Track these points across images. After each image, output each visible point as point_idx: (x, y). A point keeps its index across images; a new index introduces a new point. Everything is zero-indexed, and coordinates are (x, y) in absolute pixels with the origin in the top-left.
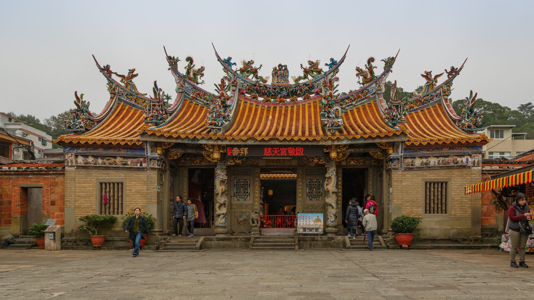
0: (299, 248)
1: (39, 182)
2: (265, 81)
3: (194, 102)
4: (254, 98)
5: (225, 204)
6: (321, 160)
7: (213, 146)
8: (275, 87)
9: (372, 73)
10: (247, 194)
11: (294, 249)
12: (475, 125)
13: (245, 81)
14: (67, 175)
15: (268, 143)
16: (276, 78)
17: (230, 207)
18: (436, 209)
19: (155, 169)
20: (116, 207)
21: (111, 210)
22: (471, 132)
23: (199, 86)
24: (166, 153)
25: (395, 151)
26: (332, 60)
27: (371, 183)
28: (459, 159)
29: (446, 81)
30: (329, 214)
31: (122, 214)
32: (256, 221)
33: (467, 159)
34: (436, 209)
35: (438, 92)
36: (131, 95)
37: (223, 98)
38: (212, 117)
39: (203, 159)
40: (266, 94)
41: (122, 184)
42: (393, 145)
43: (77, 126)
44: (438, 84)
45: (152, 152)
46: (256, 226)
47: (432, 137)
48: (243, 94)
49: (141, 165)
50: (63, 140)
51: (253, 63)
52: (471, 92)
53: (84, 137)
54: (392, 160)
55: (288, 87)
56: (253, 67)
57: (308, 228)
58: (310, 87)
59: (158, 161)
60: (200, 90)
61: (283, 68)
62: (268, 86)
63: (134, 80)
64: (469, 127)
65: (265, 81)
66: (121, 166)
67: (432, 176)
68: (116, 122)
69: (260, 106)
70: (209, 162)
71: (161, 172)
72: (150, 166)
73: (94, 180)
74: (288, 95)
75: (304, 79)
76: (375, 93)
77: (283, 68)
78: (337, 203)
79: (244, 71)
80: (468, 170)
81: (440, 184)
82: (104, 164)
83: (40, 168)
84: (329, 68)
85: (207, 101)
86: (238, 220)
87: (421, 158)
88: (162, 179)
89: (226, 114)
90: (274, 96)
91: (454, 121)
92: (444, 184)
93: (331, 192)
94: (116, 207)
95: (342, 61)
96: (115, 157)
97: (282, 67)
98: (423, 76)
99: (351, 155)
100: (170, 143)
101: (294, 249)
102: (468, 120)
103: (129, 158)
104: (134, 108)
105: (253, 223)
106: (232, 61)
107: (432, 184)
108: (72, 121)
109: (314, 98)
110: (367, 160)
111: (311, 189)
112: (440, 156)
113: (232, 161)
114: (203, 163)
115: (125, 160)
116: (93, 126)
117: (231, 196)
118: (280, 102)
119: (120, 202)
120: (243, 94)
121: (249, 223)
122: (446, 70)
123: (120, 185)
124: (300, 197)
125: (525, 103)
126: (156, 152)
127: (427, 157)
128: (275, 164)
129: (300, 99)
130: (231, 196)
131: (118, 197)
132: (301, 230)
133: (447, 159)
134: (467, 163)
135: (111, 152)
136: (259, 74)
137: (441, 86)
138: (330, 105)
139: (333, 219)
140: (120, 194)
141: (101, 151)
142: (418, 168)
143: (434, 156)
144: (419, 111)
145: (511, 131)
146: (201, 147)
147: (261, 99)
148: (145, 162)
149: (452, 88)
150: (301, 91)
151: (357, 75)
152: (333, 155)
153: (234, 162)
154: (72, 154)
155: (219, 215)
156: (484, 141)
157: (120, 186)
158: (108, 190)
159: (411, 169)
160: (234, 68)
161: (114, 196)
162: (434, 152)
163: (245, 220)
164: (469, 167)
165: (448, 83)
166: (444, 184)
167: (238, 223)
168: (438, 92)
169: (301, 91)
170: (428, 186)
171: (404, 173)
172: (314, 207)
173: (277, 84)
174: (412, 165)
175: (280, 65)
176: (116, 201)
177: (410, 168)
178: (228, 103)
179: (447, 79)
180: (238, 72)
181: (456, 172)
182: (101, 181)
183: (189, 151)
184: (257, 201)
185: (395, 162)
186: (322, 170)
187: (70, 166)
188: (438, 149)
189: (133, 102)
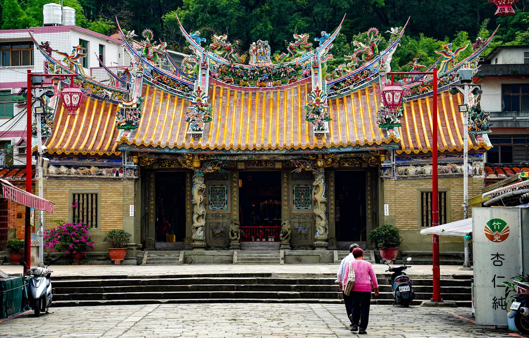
3: (155, 89)
5: (203, 215)
6: (308, 167)
11: (279, 263)
19: (132, 179)
20: (90, 219)
27: (369, 188)
30: (317, 225)
31: (96, 227)
32: (235, 234)
41: (96, 195)
42: (385, 152)
45: (128, 161)
46: (236, 239)
49: (117, 175)
66: (97, 176)
72: (127, 176)
73: (67, 191)
78: (327, 213)
82: (78, 174)
86: (213, 233)
87: (416, 166)
92: (443, 195)
94: (90, 219)
96: (89, 167)
101: (279, 263)
103: (104, 167)
105: (233, 235)
109: (302, 82)
114: (172, 166)
115: (100, 170)
117: (206, 205)
119: (94, 214)
123: (95, 197)
124: (285, 206)
126: (132, 161)
127: (422, 166)
128: (255, 167)
131: (83, 209)
133: (444, 167)
135: (88, 162)
139: (322, 231)
140: (94, 214)
141: (75, 161)
142: (413, 177)
148: (122, 172)
150: (286, 72)
155: (197, 228)
157: (94, 197)
163: (222, 232)
166: (443, 195)
167: (214, 235)
169: (286, 72)
170: (425, 196)
171: (397, 182)
172: (302, 217)
173: (257, 65)
174: (406, 174)
177: (404, 177)
182: (74, 192)
184: (235, 210)
185: (387, 171)
186: (310, 177)
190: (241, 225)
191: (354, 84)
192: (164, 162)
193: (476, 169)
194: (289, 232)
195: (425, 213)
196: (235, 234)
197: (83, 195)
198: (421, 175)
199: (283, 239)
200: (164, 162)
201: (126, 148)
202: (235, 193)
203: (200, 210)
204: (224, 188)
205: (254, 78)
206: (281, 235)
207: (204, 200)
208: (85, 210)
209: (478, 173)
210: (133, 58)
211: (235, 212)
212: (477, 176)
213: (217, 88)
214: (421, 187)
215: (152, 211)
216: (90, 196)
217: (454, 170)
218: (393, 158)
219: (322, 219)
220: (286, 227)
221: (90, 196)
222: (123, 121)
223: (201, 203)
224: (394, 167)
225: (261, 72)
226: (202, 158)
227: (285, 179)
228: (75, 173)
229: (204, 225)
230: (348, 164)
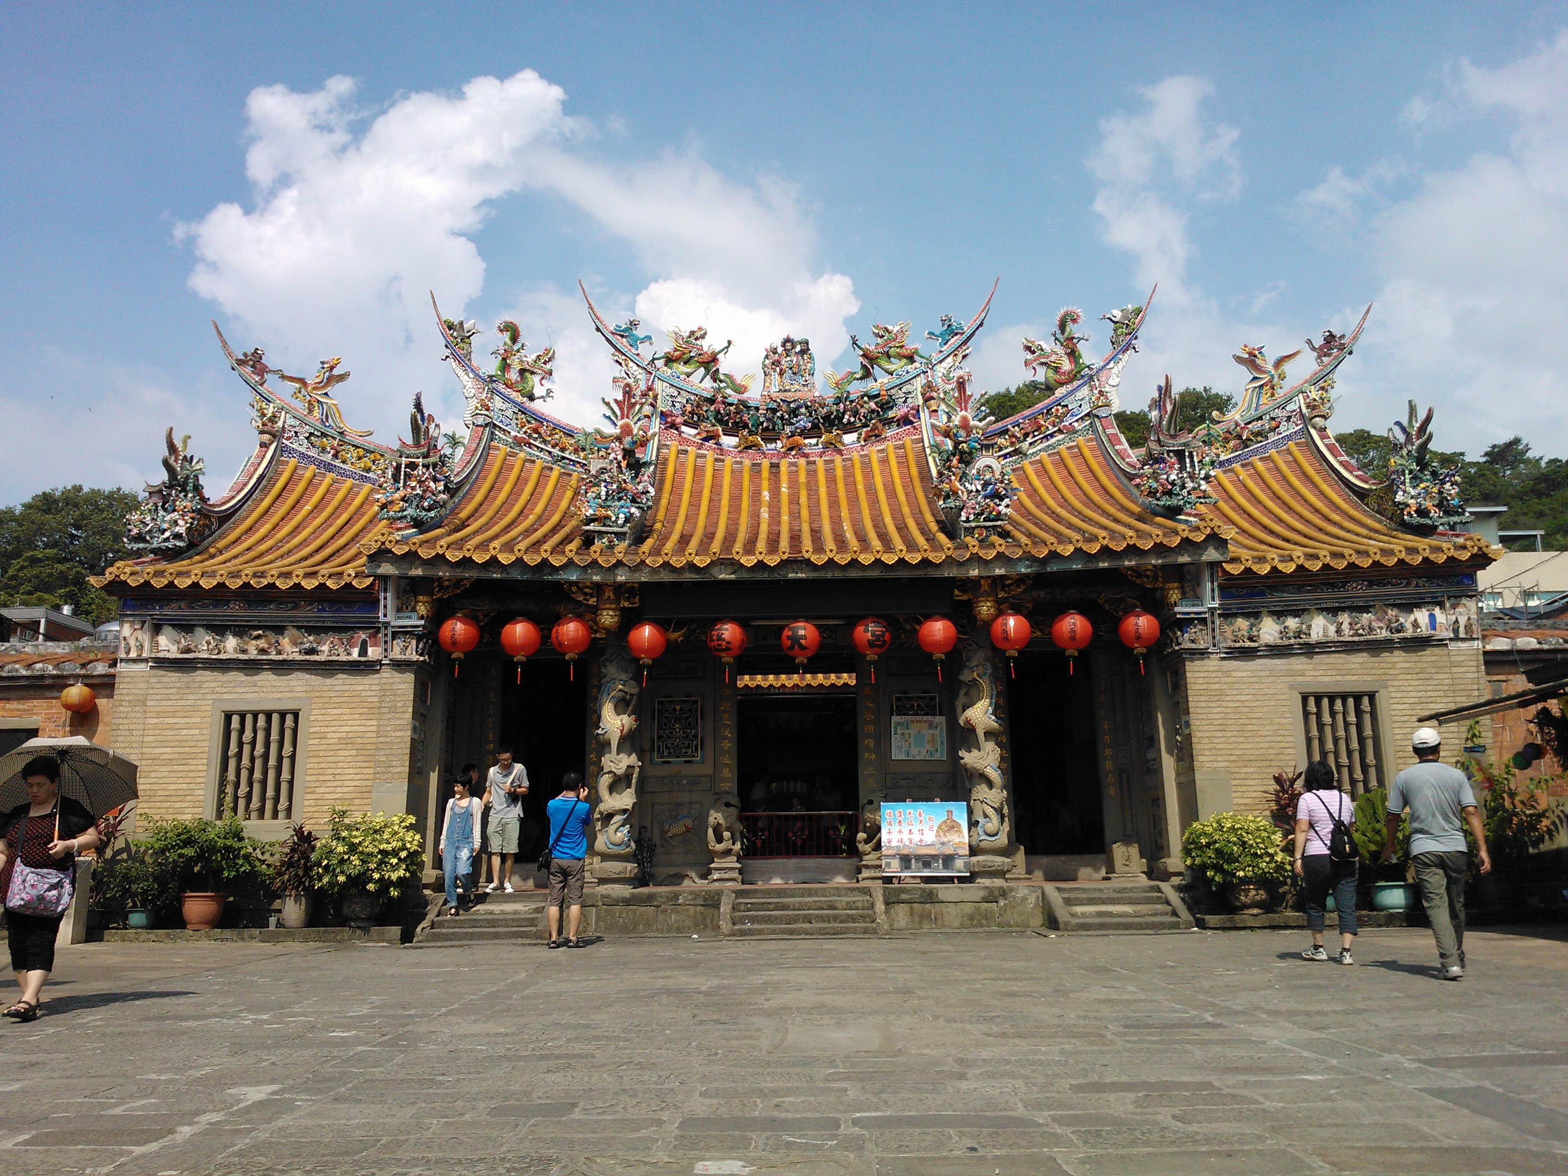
1: (30, 713)
4: (707, 439)
8: (774, 405)
9: (1073, 354)
12: (1439, 506)
14: (122, 688)
16: (775, 376)
20: (270, 793)
21: (255, 804)
23: (537, 406)
25: (1189, 594)
33: (1432, 617)
36: (324, 435)
37: (628, 439)
38: (598, 496)
40: (746, 426)
43: (163, 531)
45: (399, 610)
46: (728, 852)
47: (1257, 550)
48: (674, 426)
49: (363, 652)
50: (122, 578)
51: (703, 337)
52: (1412, 409)
53: (192, 573)
54: (1185, 623)
56: (705, 349)
57: (918, 858)
60: (540, 419)
62: (751, 403)
63: (338, 393)
65: (740, 389)
69: (729, 460)
72: (392, 656)
74: (815, 426)
76: (1088, 415)
77: (798, 348)
79: (676, 360)
80: (1436, 650)
82: (244, 651)
83: (39, 666)
85: (563, 450)
88: (426, 696)
90: (770, 435)
91: (1362, 495)
94: (270, 793)
97: (793, 347)
98: (1239, 360)
102: (1413, 492)
104: (330, 476)
105: (719, 839)
107: (1325, 702)
108: (148, 518)
118: (791, 449)
119: (285, 775)
122: (1309, 342)
125: (1503, 438)
126: (414, 610)
129: (849, 438)
131: (280, 759)
132: (895, 864)
135: (269, 613)
136: (725, 366)
138: (962, 452)
141: (236, 611)
143: (1322, 610)
144: (1237, 466)
145: (1493, 524)
147: (729, 441)
150: (855, 413)
155: (608, 817)
156: (1483, 560)
158: (248, 736)
161: (266, 756)
163: (688, 830)
164: (1441, 643)
168: (1291, 407)
170: (1312, 707)
174: (1251, 639)
176: (271, 774)
180: (660, 363)
181: (1399, 659)
182: (230, 708)
185: (1193, 631)
187: (134, 661)
188: (1333, 585)
189: (328, 458)
190: (742, 810)
191: (1029, 440)
193: (1457, 621)
201: (387, 569)
206: (861, 836)
210: (469, 385)
213: (679, 452)
214: (1300, 679)
219: (990, 784)
222: (397, 496)
226: (627, 599)
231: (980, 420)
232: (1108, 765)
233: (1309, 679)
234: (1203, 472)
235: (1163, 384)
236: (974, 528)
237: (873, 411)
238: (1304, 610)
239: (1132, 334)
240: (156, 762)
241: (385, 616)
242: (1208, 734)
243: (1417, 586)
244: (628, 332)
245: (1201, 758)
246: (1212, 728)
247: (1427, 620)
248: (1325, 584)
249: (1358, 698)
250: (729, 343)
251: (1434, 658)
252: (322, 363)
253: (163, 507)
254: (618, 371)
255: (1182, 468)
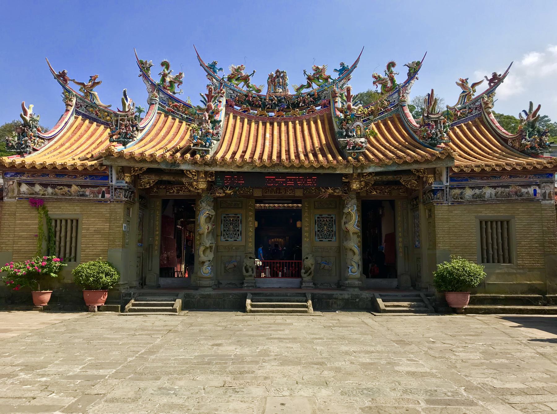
0: (194, 204)
2: (259, 91)
4: (244, 112)
6: (337, 191)
7: (198, 172)
9: (392, 80)
10: (237, 233)
13: (234, 91)
15: (270, 170)
17: (217, 250)
18: (496, 257)
22: (536, 156)
24: (136, 180)
26: (342, 64)
27: (399, 218)
28: (524, 190)
29: (487, 90)
31: (75, 261)
32: (250, 269)
33: (535, 190)
34: (496, 257)
35: (477, 104)
36: (92, 107)
39: (181, 188)
40: (260, 106)
41: (77, 221)
44: (476, 94)
45: (117, 179)
46: (251, 276)
48: (231, 106)
49: (103, 196)
52: (531, 104)
55: (286, 98)
58: (315, 99)
59: (126, 190)
61: (282, 75)
64: (532, 148)
65: (259, 91)
67: (488, 213)
68: (72, 140)
70: (190, 191)
71: (129, 205)
72: (115, 197)
75: (307, 88)
76: (397, 105)
81: (499, 223)
82: (56, 194)
84: (339, 75)
86: (225, 267)
87: (472, 188)
88: (129, 214)
89: (215, 132)
92: (505, 223)
93: (351, 233)
95: (354, 66)
96: (70, 186)
97: (280, 74)
99: (376, 183)
100: (141, 169)
103: (88, 187)
105: (247, 271)
106: (218, 66)
109: (320, 111)
110: (394, 189)
111: (320, 226)
112: (498, 187)
113: (221, 191)
114: (181, 193)
116: (43, 145)
117: (217, 236)
119: (73, 244)
120: (231, 106)
121: (241, 271)
122: (486, 77)
126: (123, 179)
127: (480, 188)
128: (273, 194)
130: (217, 236)
131: (71, 238)
134: (535, 195)
135: (65, 180)
136: (252, 82)
137: (481, 97)
143: (490, 187)
146: (182, 173)
149: (494, 99)
150: (304, 102)
151: (374, 83)
152: (355, 186)
153: (224, 192)
154: (13, 182)
155: (203, 262)
159: (460, 203)
160: (219, 75)
162: (489, 181)
165: (490, 92)
166: (505, 223)
168: (477, 104)
174: (461, 198)
175: (278, 71)
177: (459, 201)
178: (217, 118)
179: (488, 87)
183: (166, 178)
184: (250, 242)
185: (439, 194)
186: (338, 204)
187: (10, 198)
188: (495, 177)
192: (172, 189)
194: (313, 268)
195: (485, 247)
196: (250, 269)
197: (61, 221)
198: (479, 199)
199: (305, 275)
200: (172, 189)
202: (251, 223)
203: (208, 242)
204: (238, 217)
205: (271, 108)
207: (213, 229)
208: (63, 239)
209: (547, 198)
211: (250, 244)
212: (546, 202)
215: (157, 243)
216: (69, 222)
217: (519, 194)
218: (447, 178)
219: (354, 253)
220: (309, 262)
221: (69, 222)
223: (208, 233)
224: (448, 189)
225: (279, 101)
226: (210, 177)
227: (306, 208)
228: (52, 193)
229: (211, 259)
230: (376, 192)
231: (356, 106)
232: (400, 245)
233: (483, 214)
234: (445, 130)
235: (430, 93)
236: (351, 153)
237: (311, 101)
238: (483, 187)
239: (416, 72)
240: (20, 238)
241: (111, 182)
242: (442, 236)
243: (530, 178)
244: (213, 66)
245: (439, 245)
246: (444, 233)
247: (533, 192)
248: (492, 177)
249: (502, 222)
250: (254, 72)
251: (534, 207)
252: (91, 77)
253: (22, 134)
254: (209, 82)
255: (437, 128)
